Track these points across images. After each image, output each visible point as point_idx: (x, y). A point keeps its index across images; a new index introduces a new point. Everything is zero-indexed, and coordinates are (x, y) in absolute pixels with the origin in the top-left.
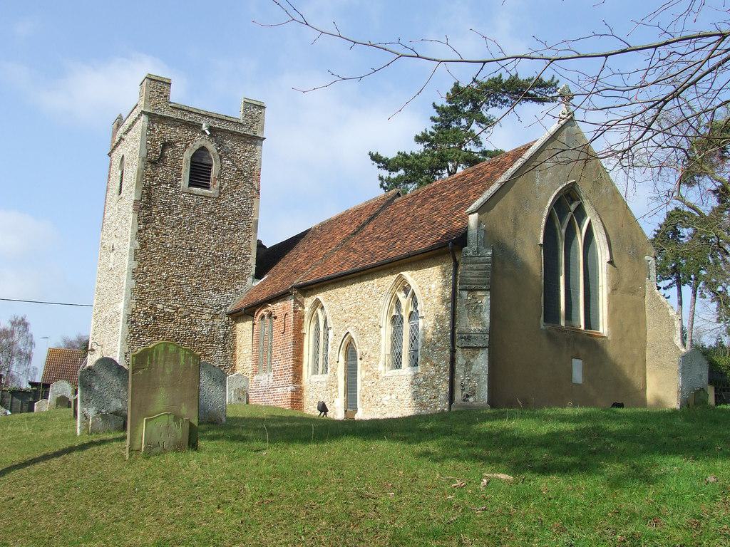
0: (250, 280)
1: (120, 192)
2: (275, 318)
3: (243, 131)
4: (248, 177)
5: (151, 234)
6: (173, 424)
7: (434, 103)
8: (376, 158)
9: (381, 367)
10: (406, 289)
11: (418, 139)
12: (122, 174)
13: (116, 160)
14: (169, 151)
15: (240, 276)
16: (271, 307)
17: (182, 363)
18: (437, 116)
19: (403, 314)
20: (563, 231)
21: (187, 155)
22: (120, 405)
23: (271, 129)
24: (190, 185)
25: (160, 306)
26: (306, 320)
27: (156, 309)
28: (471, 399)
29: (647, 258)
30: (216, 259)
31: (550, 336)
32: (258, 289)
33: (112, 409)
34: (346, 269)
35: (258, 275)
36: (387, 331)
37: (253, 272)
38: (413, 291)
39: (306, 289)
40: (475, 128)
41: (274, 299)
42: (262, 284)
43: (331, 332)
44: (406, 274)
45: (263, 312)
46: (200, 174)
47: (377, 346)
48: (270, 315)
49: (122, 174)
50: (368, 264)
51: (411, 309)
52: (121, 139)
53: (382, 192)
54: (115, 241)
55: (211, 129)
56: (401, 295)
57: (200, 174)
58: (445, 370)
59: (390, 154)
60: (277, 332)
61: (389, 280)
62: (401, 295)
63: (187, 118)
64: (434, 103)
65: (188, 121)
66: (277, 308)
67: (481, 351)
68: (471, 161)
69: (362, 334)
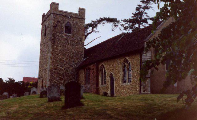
5: (55, 47)
14: (59, 24)
25: (58, 66)
43: (106, 73)
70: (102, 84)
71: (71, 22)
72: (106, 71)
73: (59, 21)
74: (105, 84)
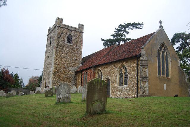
0: (80, 64)
1: (50, 44)
2: (88, 73)
3: (79, 31)
4: (80, 41)
6: (100, 104)
7: (115, 28)
8: (103, 40)
9: (117, 85)
10: (124, 67)
11: (111, 36)
12: (51, 40)
13: (49, 37)
14: (62, 35)
15: (78, 64)
16: (87, 71)
17: (102, 85)
18: (116, 31)
19: (123, 72)
20: (161, 54)
21: (66, 36)
22: (68, 96)
23: (85, 30)
24: (67, 43)
25: (60, 70)
26: (96, 74)
27: (59, 71)
28: (144, 94)
29: (178, 61)
30: (72, 59)
31: (159, 78)
32: (82, 66)
33: (65, 97)
34: (107, 62)
35: (82, 64)
36: (118, 77)
37: (81, 63)
38: (126, 67)
39: (96, 67)
40: (125, 33)
41: (87, 69)
42: (83, 66)
43: (103, 77)
44: (124, 63)
45: (85, 72)
46: (69, 40)
47: (116, 80)
48: (87, 73)
49: (51, 40)
50: (114, 60)
51: (125, 71)
52: (51, 32)
53: (104, 47)
54: (49, 55)
55: (72, 30)
56: (122, 68)
57: (69, 40)
58: (135, 86)
59: (105, 39)
60: (88, 76)
61: (119, 65)
62: (122, 68)
63: (66, 28)
64: (115, 28)
65: (67, 28)
66: (89, 71)
67: (147, 82)
68: (124, 40)
69: (112, 77)
70: (121, 84)
71: (72, 34)
72: (103, 75)
73: (62, 33)
74: (126, 84)
